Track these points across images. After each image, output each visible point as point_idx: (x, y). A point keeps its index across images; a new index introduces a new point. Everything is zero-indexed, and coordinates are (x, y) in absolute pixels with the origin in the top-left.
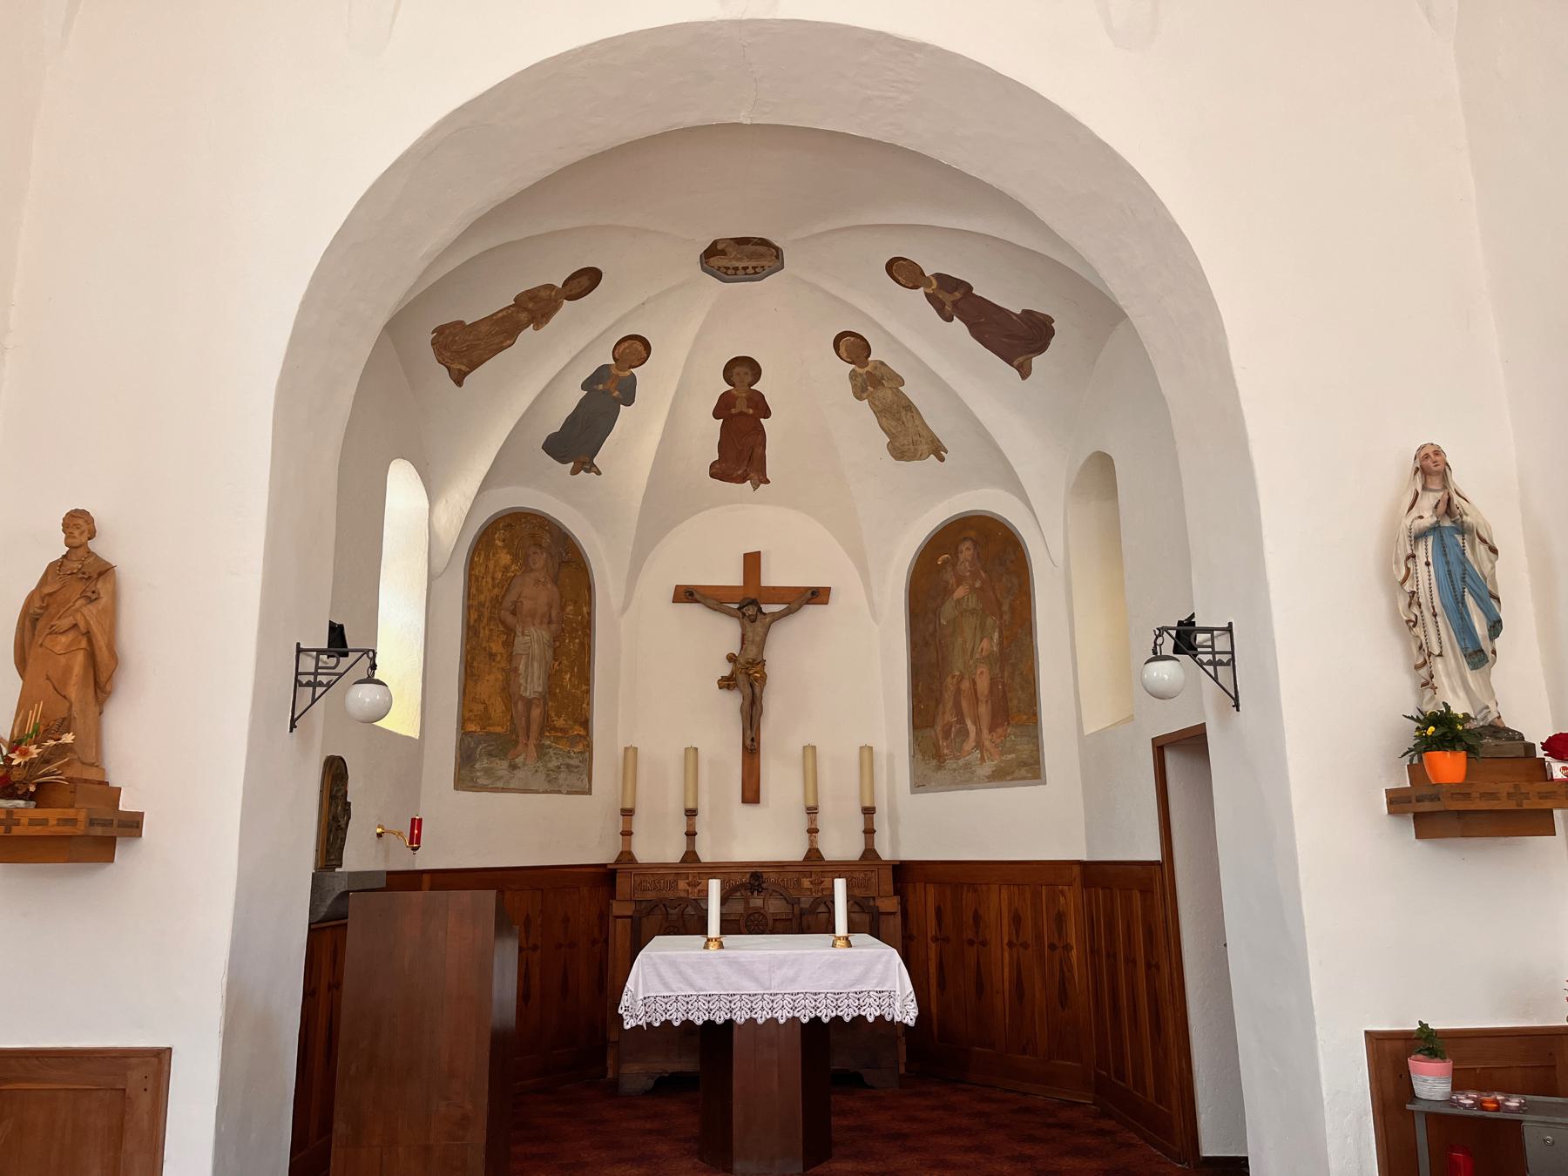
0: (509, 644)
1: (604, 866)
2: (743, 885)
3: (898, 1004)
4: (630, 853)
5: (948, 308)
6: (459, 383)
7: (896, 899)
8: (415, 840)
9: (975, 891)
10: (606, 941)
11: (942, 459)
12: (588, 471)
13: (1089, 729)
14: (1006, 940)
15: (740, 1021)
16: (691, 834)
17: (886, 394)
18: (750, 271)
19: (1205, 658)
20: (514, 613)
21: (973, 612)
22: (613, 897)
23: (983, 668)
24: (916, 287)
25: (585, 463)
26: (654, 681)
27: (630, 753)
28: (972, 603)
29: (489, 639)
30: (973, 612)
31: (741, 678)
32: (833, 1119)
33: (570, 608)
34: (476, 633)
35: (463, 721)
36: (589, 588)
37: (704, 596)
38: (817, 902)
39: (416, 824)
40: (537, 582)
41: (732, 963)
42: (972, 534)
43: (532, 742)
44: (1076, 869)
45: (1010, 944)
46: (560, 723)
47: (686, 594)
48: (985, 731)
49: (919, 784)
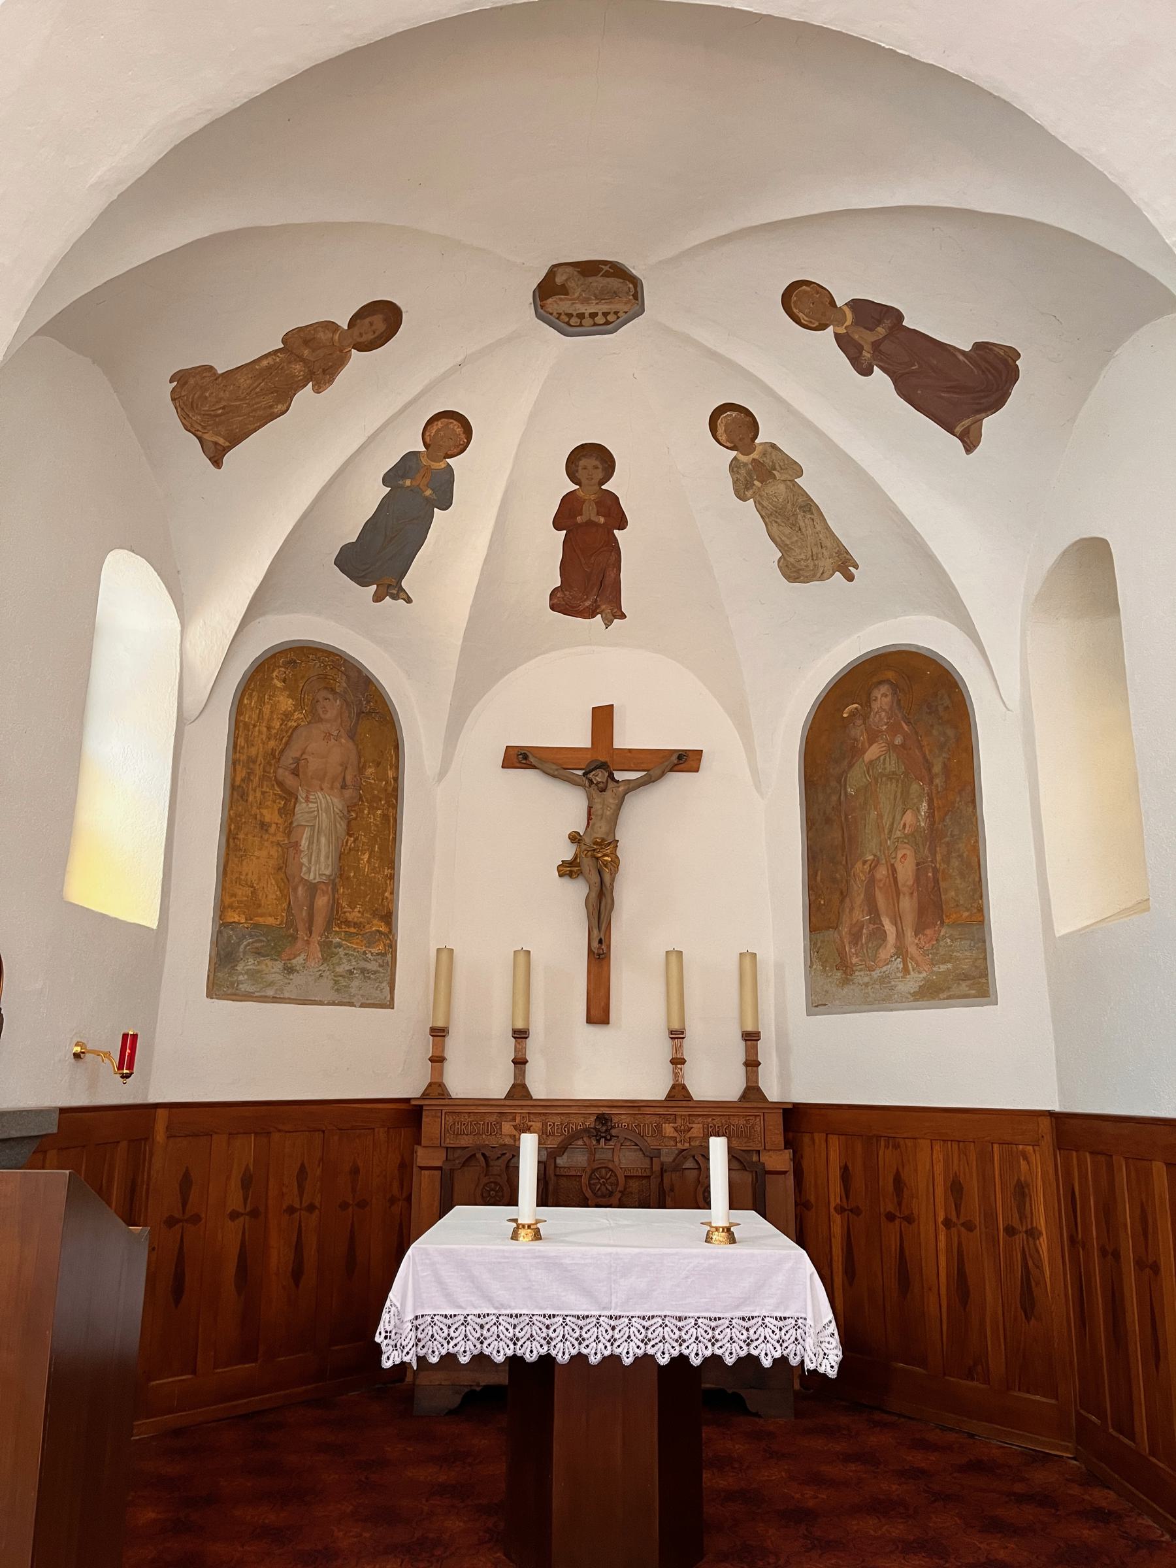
0: (287, 812)
1: (407, 1101)
2: (586, 1130)
3: (810, 1342)
5: (867, 355)
6: (217, 462)
7: (788, 1154)
8: (127, 1059)
9: (897, 1146)
11: (850, 578)
12: (395, 597)
13: (1061, 930)
14: (941, 1218)
16: (520, 1062)
17: (778, 490)
18: (600, 319)
20: (295, 773)
21: (891, 777)
22: (419, 1143)
23: (907, 851)
24: (822, 327)
26: (476, 866)
27: (444, 956)
28: (891, 765)
29: (260, 806)
30: (891, 777)
31: (587, 863)
32: (706, 1475)
33: (370, 771)
34: (243, 796)
35: (222, 908)
36: (397, 746)
39: (129, 1043)
40: (328, 736)
42: (890, 675)
45: (948, 1223)
46: (354, 915)
47: (519, 758)
48: (909, 933)
49: (817, 1004)
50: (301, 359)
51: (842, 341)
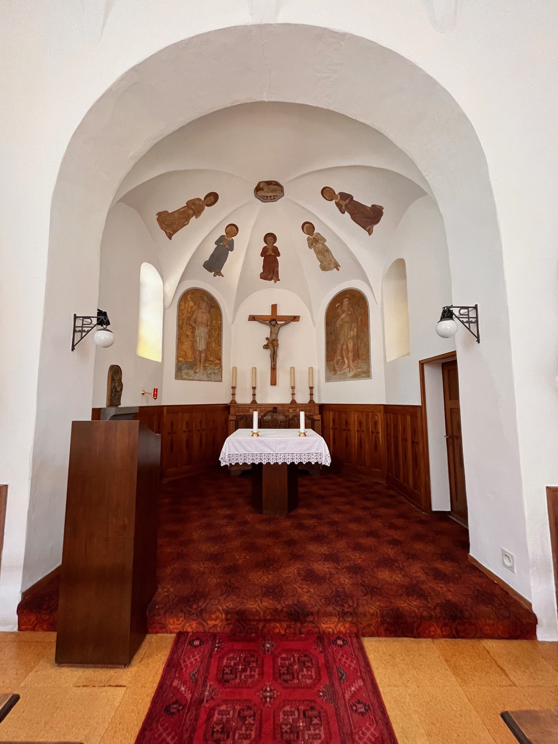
0: (193, 332)
3: (323, 458)
4: (235, 401)
5: (343, 208)
6: (170, 238)
7: (320, 416)
8: (155, 396)
10: (227, 428)
11: (338, 270)
14: (356, 430)
15: (264, 463)
16: (254, 395)
17: (320, 246)
18: (272, 198)
19: (465, 320)
20: (195, 322)
24: (331, 200)
25: (218, 273)
26: (242, 346)
28: (347, 319)
29: (186, 331)
31: (270, 345)
32: (299, 489)
33: (214, 322)
34: (182, 329)
35: (178, 357)
37: (258, 319)
38: (294, 416)
39: (156, 390)
41: (262, 442)
42: (348, 296)
43: (202, 365)
44: (382, 407)
45: (358, 431)
46: (211, 359)
47: (252, 318)
48: (351, 362)
50: (191, 209)
51: (337, 204)
